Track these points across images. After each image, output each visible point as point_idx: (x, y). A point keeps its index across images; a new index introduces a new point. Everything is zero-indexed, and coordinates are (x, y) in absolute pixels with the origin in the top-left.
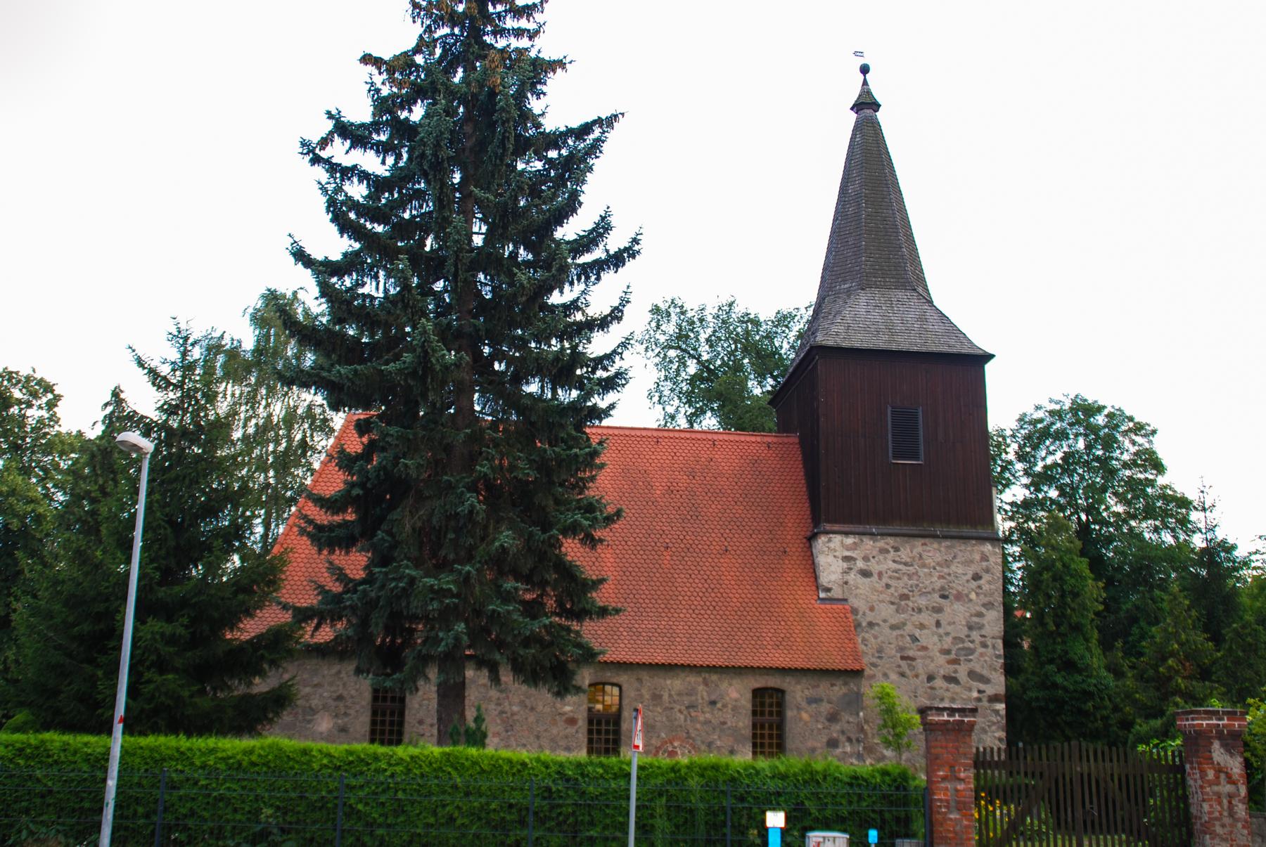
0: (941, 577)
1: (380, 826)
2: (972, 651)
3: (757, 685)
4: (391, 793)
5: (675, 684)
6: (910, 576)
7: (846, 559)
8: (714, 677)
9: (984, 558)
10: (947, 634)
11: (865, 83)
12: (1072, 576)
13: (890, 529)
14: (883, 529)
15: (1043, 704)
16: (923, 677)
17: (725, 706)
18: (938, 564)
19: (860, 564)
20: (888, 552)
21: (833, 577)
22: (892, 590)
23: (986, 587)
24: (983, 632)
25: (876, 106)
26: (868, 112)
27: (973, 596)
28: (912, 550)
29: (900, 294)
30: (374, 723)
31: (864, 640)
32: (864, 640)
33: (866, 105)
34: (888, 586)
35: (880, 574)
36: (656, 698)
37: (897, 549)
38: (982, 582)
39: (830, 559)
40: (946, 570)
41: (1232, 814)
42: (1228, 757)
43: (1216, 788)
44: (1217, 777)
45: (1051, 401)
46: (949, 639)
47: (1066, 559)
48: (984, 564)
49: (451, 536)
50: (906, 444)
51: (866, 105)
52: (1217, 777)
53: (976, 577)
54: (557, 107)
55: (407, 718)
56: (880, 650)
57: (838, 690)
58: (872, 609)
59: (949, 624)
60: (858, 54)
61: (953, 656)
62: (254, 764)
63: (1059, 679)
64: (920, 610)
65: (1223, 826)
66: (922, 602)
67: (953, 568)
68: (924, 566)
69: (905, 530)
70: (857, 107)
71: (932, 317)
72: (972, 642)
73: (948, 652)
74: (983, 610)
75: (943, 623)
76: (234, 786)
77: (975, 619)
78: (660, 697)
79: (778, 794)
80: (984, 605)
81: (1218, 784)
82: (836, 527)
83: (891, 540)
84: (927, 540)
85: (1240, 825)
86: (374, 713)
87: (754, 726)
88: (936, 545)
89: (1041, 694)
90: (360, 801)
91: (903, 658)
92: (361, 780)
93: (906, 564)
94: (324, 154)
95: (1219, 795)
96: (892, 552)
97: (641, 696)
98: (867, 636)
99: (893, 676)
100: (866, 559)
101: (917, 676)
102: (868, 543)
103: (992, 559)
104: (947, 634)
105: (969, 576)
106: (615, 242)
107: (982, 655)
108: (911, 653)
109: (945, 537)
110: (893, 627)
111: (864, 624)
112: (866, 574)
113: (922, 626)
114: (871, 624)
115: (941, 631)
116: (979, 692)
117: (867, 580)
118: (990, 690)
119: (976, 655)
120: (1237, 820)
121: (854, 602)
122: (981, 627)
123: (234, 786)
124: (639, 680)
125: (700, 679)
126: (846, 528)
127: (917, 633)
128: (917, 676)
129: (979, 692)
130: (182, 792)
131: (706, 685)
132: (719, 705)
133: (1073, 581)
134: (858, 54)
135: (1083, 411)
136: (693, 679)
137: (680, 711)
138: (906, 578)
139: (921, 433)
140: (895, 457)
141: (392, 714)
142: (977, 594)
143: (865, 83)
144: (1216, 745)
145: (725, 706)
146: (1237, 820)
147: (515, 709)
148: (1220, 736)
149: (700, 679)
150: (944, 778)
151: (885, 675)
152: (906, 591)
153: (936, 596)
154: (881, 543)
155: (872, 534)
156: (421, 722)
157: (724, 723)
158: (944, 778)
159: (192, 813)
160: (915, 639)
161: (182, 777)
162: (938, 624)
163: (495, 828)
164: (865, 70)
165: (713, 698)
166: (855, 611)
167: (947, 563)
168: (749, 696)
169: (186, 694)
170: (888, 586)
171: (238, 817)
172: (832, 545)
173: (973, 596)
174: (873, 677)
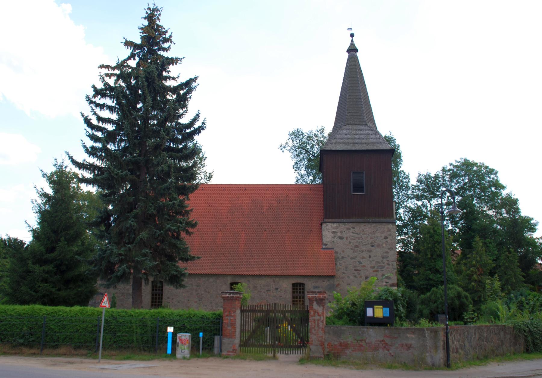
0: (371, 238)
1: (57, 332)
2: (383, 267)
3: (294, 282)
4: (62, 322)
5: (262, 282)
6: (359, 238)
7: (333, 232)
8: (277, 279)
9: (389, 230)
10: (374, 260)
11: (352, 41)
12: (438, 235)
13: (351, 220)
14: (348, 220)
15: (425, 286)
16: (364, 277)
17: (281, 290)
18: (370, 233)
19: (339, 234)
20: (350, 229)
21: (328, 240)
22: (352, 244)
23: (390, 242)
24: (388, 259)
25: (356, 50)
26: (352, 53)
27: (384, 245)
28: (359, 228)
29: (360, 127)
30: (152, 298)
31: (340, 263)
32: (340, 263)
33: (352, 50)
34: (350, 242)
35: (347, 238)
36: (255, 287)
37: (354, 228)
38: (388, 240)
39: (327, 233)
40: (373, 235)
41: (318, 326)
42: (318, 307)
43: (314, 318)
44: (314, 314)
45: (456, 161)
46: (374, 262)
47: (436, 228)
48: (389, 232)
49: (127, 234)
50: (358, 187)
51: (352, 50)
52: (314, 314)
53: (386, 238)
54: (177, 74)
55: (163, 297)
56: (346, 268)
57: (325, 283)
58: (343, 252)
59: (375, 256)
60: (349, 29)
61: (376, 269)
62: (24, 314)
63: (431, 277)
64: (363, 252)
65: (315, 330)
66: (364, 248)
67: (376, 234)
68: (364, 234)
69: (358, 220)
70: (349, 51)
71: (372, 134)
72: (383, 263)
73: (374, 267)
74: (388, 250)
75: (372, 256)
76: (17, 321)
77: (385, 254)
78: (257, 287)
79: (177, 321)
80: (389, 249)
81: (315, 316)
82: (330, 220)
83: (351, 225)
84: (365, 224)
85: (320, 330)
86: (153, 295)
87: (293, 297)
88: (369, 226)
89: (425, 283)
90: (53, 325)
91: (355, 270)
92: (54, 318)
93: (357, 234)
94: (94, 100)
95: (314, 320)
96: (352, 229)
97: (249, 287)
98: (341, 262)
99: (352, 277)
100: (341, 232)
101: (361, 277)
102: (342, 226)
103: (392, 231)
104: (374, 260)
105: (383, 238)
106: (197, 125)
107: (387, 268)
108: (359, 268)
109: (373, 223)
110: (352, 258)
111: (340, 257)
112: (341, 238)
113: (363, 258)
114: (343, 258)
115: (371, 259)
116: (386, 282)
117: (341, 240)
118: (391, 282)
119: (385, 268)
120: (319, 328)
121: (336, 249)
122: (387, 257)
123: (17, 321)
124: (249, 281)
125: (272, 280)
126: (334, 220)
127: (361, 260)
128: (361, 277)
129: (386, 282)
130: (3, 323)
131: (274, 282)
132: (279, 290)
133: (438, 237)
134: (349, 29)
135: (467, 165)
136: (269, 280)
137: (264, 292)
138: (357, 239)
139: (364, 182)
140: (354, 192)
141: (159, 295)
142: (386, 244)
143: (352, 41)
144: (315, 303)
145: (281, 290)
146: (319, 328)
147: (203, 292)
148: (316, 300)
149: (272, 280)
150: (227, 316)
151: (348, 277)
152: (357, 244)
153: (369, 245)
154: (348, 226)
155: (344, 223)
156: (168, 298)
157: (281, 296)
158: (227, 316)
159: (5, 330)
160: (360, 263)
161: (4, 318)
162: (370, 257)
163: (90, 333)
164: (352, 35)
165: (277, 287)
166: (336, 253)
167: (374, 233)
168: (291, 286)
169: (54, 290)
170: (350, 242)
171: (18, 330)
172: (328, 227)
173: (384, 245)
174: (343, 278)
